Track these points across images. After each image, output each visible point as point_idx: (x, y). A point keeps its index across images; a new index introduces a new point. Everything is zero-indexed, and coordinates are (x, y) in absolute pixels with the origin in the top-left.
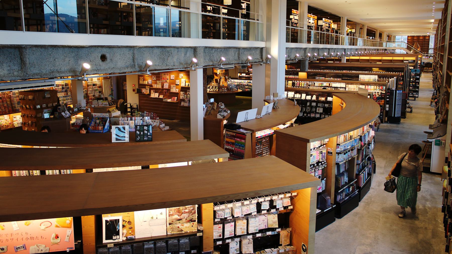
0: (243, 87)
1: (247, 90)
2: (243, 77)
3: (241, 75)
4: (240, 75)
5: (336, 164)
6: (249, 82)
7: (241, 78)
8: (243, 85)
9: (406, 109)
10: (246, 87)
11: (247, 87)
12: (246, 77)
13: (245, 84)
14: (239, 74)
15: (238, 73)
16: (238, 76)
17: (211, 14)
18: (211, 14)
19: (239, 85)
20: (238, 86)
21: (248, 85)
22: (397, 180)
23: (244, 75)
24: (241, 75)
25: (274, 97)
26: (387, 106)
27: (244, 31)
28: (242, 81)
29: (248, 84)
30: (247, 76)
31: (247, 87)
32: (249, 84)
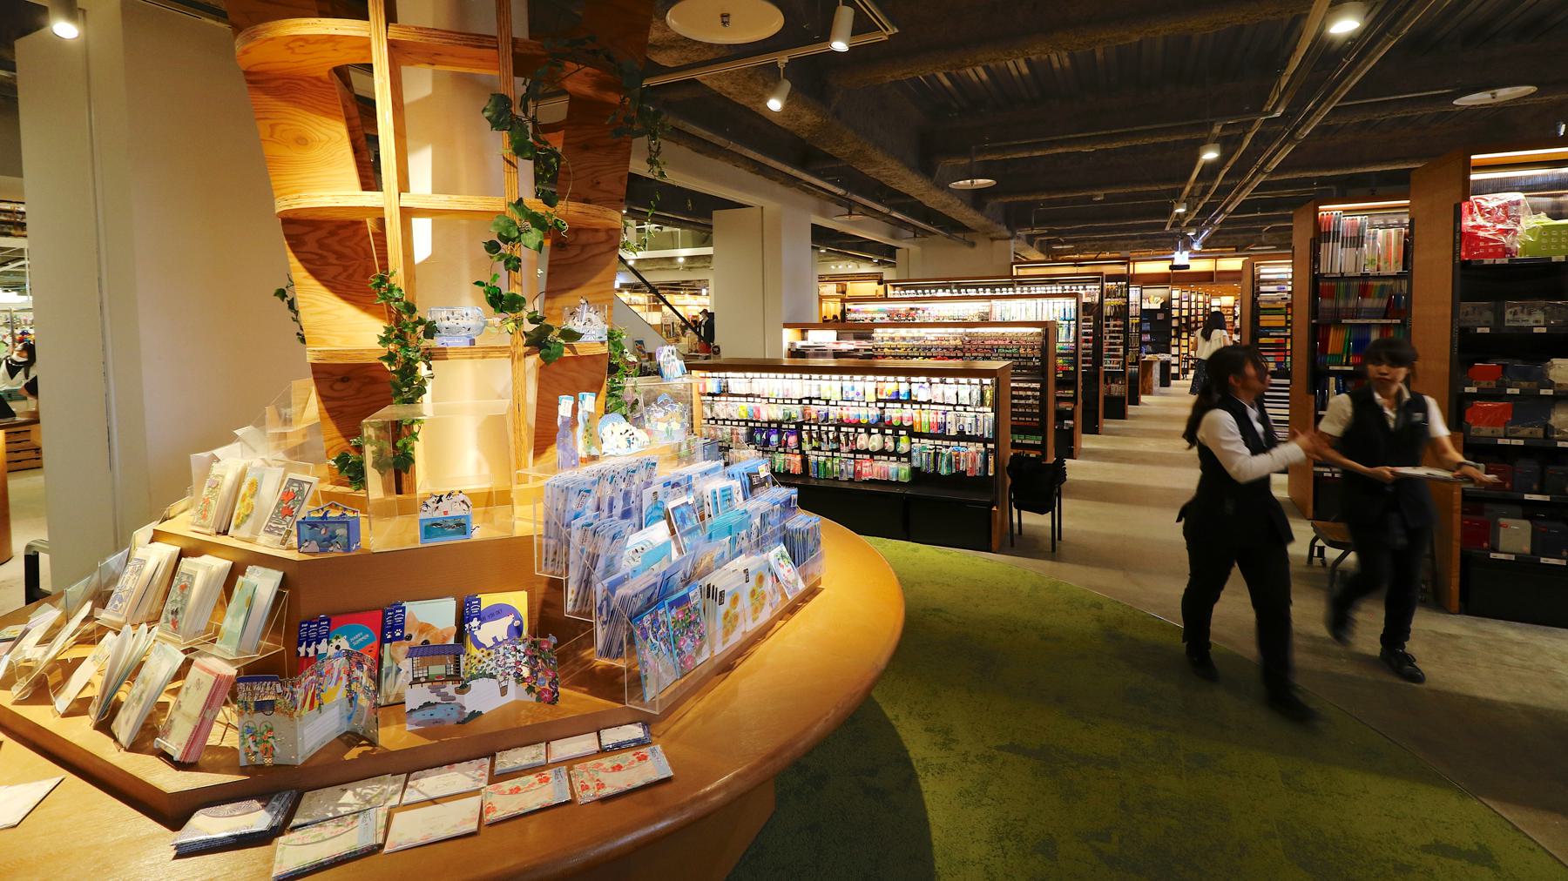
0: (837, 439)
1: (873, 469)
2: (820, 352)
3: (804, 339)
4: (799, 344)
5: (1168, 385)
6: (896, 399)
7: (800, 362)
8: (839, 424)
9: (1404, 647)
10: (863, 441)
11: (875, 442)
12: (838, 354)
13: (851, 412)
14: (790, 337)
15: (787, 326)
16: (786, 346)
17: (1080, 390)
18: (1080, 390)
19: (799, 426)
20: (791, 432)
21: (882, 424)
22: (1149, 427)
23: (825, 338)
24: (804, 343)
25: (23, 203)
26: (1550, 392)
27: (850, 214)
28: (829, 386)
29: (881, 419)
30: (846, 346)
31: (875, 442)
32: (894, 413)
